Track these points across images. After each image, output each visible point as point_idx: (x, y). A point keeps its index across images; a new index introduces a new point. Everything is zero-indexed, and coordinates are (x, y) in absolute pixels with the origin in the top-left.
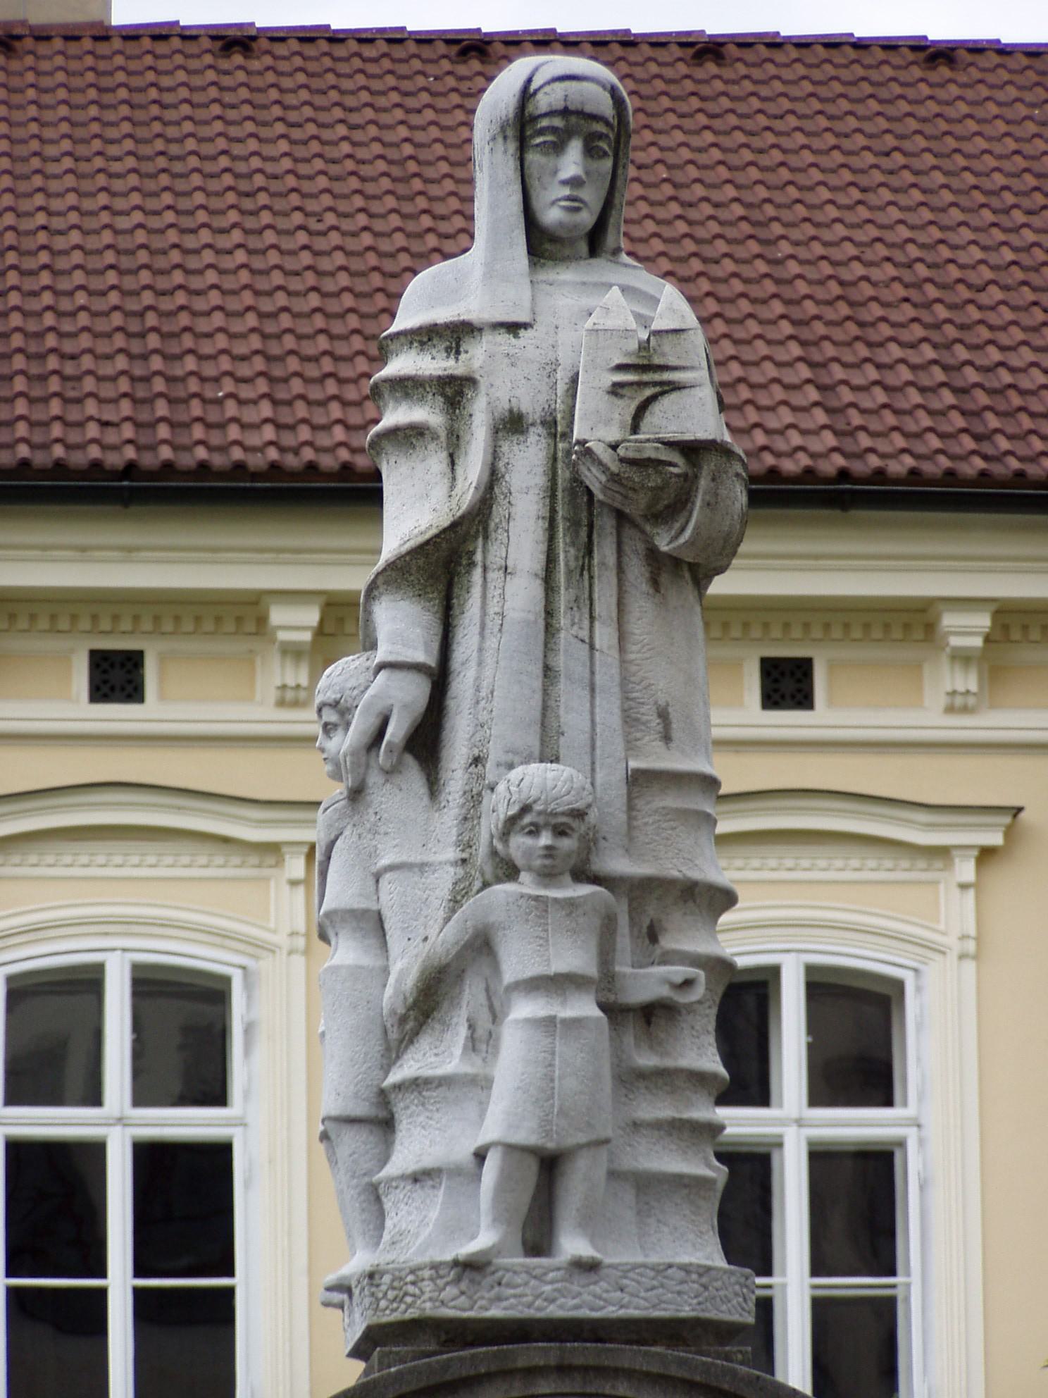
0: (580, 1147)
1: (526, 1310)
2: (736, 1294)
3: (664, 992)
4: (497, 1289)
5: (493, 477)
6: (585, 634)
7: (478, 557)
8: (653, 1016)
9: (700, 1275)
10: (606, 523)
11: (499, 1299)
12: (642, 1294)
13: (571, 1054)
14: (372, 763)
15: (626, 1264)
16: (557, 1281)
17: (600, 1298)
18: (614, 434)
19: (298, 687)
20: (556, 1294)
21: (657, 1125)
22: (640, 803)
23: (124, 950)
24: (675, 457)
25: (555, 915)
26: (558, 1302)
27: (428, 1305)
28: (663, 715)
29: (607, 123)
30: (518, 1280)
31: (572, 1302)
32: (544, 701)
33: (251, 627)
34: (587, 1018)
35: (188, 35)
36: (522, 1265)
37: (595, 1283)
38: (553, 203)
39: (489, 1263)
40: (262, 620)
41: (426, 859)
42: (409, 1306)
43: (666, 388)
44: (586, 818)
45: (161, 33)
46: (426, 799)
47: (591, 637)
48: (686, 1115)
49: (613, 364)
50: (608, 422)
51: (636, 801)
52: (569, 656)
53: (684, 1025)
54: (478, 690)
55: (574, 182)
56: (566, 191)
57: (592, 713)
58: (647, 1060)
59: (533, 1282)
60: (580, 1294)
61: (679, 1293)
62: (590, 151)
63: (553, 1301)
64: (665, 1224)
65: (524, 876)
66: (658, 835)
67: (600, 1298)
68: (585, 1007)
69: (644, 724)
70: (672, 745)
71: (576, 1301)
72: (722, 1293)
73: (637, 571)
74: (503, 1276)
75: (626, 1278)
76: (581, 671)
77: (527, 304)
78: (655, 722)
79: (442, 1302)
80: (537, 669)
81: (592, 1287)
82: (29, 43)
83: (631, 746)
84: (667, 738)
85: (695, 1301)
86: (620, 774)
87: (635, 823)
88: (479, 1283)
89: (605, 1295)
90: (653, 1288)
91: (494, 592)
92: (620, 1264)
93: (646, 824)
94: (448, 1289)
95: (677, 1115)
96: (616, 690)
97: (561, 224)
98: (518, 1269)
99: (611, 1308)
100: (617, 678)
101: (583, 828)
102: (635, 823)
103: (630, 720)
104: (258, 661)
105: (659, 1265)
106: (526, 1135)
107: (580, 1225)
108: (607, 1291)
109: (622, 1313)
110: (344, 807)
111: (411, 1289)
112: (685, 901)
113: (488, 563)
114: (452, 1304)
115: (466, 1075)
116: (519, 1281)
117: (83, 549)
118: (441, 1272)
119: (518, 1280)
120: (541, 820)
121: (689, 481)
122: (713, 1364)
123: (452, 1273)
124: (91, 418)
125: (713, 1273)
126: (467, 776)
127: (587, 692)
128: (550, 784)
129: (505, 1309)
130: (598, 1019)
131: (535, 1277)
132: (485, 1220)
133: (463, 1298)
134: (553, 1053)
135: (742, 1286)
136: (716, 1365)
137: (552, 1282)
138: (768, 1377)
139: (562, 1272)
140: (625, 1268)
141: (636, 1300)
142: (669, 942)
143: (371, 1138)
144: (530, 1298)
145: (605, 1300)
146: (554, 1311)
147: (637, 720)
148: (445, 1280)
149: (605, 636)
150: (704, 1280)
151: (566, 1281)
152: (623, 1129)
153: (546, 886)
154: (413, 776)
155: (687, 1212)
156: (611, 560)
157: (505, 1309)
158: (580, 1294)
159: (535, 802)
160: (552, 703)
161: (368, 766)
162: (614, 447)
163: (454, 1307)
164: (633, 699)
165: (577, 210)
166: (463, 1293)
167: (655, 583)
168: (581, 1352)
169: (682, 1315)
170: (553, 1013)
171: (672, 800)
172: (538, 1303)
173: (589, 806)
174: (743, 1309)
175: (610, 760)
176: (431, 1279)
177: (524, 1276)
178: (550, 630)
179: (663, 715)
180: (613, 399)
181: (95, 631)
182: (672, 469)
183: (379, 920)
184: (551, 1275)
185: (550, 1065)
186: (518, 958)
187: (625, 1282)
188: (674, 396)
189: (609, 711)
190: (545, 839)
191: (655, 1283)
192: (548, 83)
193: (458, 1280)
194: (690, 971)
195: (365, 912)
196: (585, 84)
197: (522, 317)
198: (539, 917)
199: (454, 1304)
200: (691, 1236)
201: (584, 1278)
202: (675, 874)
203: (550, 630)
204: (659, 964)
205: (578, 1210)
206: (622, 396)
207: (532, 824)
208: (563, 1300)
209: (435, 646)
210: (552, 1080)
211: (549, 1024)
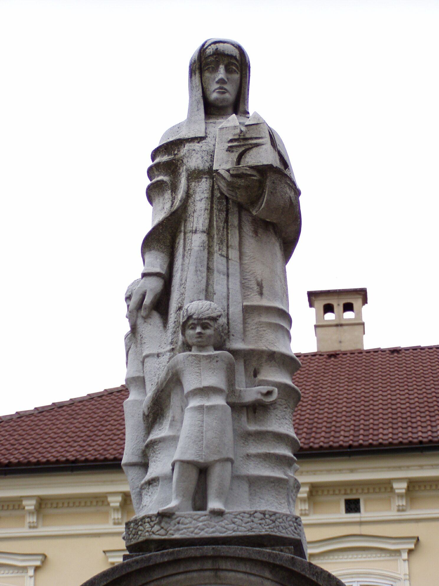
0: (216, 461)
1: (191, 534)
2: (291, 526)
3: (259, 397)
4: (177, 525)
5: (188, 195)
6: (224, 253)
7: (183, 228)
8: (257, 409)
9: (271, 516)
10: (234, 209)
11: (178, 530)
12: (243, 525)
13: (210, 421)
14: (139, 315)
15: (236, 512)
16: (205, 521)
17: (224, 527)
18: (228, 166)
19: (403, 505)
20: (204, 527)
21: (258, 456)
22: (249, 321)
23: (358, 582)
24: (254, 173)
25: (204, 362)
26: (205, 530)
27: (147, 534)
28: (260, 285)
29: (235, 58)
30: (187, 521)
31: (212, 530)
32: (207, 281)
33: (389, 490)
34: (218, 405)
35: (383, 351)
36: (189, 514)
37: (222, 521)
38: (214, 91)
39: (173, 514)
40: (392, 488)
41: (160, 351)
42: (140, 536)
43: (250, 146)
44: (218, 321)
45: (376, 351)
46: (161, 328)
47: (227, 254)
48: (272, 451)
49: (229, 140)
50: (227, 162)
51: (248, 320)
52: (219, 262)
53: (272, 414)
54: (181, 280)
55: (222, 81)
56: (217, 86)
57: (228, 285)
58: (252, 428)
59: (194, 522)
60: (215, 526)
61: (260, 524)
62: (228, 70)
63: (203, 530)
64: (263, 499)
65: (193, 349)
66: (257, 333)
67: (224, 527)
68: (219, 401)
69: (251, 289)
70: (263, 297)
71: (214, 529)
72: (282, 524)
73: (248, 229)
74: (180, 520)
75: (236, 518)
76: (223, 268)
77: (203, 130)
78: (256, 287)
79: (153, 532)
80: (204, 269)
81: (220, 523)
82: (341, 355)
83: (245, 297)
84: (261, 294)
85: (268, 527)
86: (240, 308)
87: (247, 329)
88: (169, 523)
89: (226, 526)
90: (248, 522)
91: (188, 242)
92: (232, 512)
93: (252, 329)
94: (155, 526)
95: (268, 451)
96: (238, 274)
97: (217, 99)
98: (187, 516)
99: (229, 532)
100: (238, 270)
101: (216, 326)
102: (247, 329)
103: (244, 286)
104: (392, 500)
105: (251, 511)
106: (189, 456)
107: (217, 497)
108: (227, 524)
109: (234, 534)
110: (131, 336)
111: (141, 528)
112: (271, 361)
113: (186, 231)
114: (157, 533)
115: (170, 436)
116: (188, 521)
117: (340, 470)
118: (153, 519)
119: (187, 521)
120: (196, 322)
121: (261, 184)
122: (271, 552)
123: (157, 519)
124: (342, 435)
125: (277, 515)
126: (176, 315)
127: (226, 277)
128: (200, 307)
129: (181, 534)
130: (223, 406)
131: (194, 519)
132: (174, 496)
133: (162, 530)
134: (203, 421)
135: (293, 522)
136: (273, 553)
137: (201, 522)
138: (304, 560)
139: (207, 517)
140: (236, 513)
141: (240, 528)
142: (260, 377)
143: (140, 472)
144: (192, 529)
145: (227, 529)
146: (203, 534)
147: (248, 287)
148: (154, 522)
149: (234, 254)
150: (273, 518)
151: (209, 520)
152: (242, 457)
153: (200, 351)
154: (156, 319)
155: (274, 494)
156: (236, 223)
157: (181, 534)
158: (215, 526)
159: (193, 314)
160: (211, 282)
161: (137, 317)
162: (228, 171)
163: (158, 534)
164: (246, 279)
165: (223, 93)
166: (162, 528)
167: (256, 232)
168: (208, 550)
169: (262, 533)
170: (202, 404)
171: (265, 319)
172: (196, 531)
173: (220, 316)
174: (295, 532)
175: (235, 303)
176: (148, 522)
177: (189, 519)
178: (210, 254)
179: (260, 285)
180: (228, 152)
181: (346, 494)
182: (254, 178)
183: (144, 378)
184: (202, 518)
185: (201, 426)
186: (190, 382)
187: (236, 520)
188: (255, 150)
189: (235, 284)
190: (199, 330)
191: (249, 520)
192: (210, 45)
193: (159, 523)
194: (270, 388)
195: (138, 377)
196: (225, 44)
197: (202, 135)
198: (197, 364)
199: (158, 533)
200: (276, 504)
201: (217, 519)
202: (264, 348)
203: (210, 254)
204: (258, 386)
205: (216, 490)
206: (233, 152)
207: (192, 324)
208: (207, 529)
209: (165, 266)
210: (202, 433)
211: (201, 408)
